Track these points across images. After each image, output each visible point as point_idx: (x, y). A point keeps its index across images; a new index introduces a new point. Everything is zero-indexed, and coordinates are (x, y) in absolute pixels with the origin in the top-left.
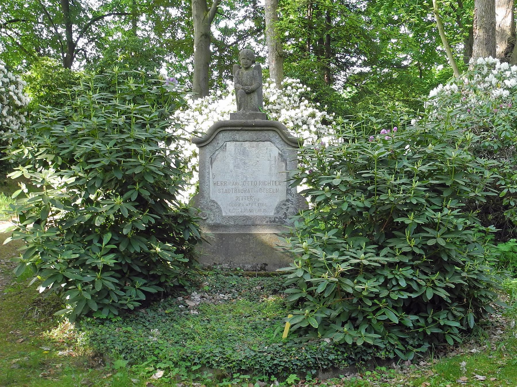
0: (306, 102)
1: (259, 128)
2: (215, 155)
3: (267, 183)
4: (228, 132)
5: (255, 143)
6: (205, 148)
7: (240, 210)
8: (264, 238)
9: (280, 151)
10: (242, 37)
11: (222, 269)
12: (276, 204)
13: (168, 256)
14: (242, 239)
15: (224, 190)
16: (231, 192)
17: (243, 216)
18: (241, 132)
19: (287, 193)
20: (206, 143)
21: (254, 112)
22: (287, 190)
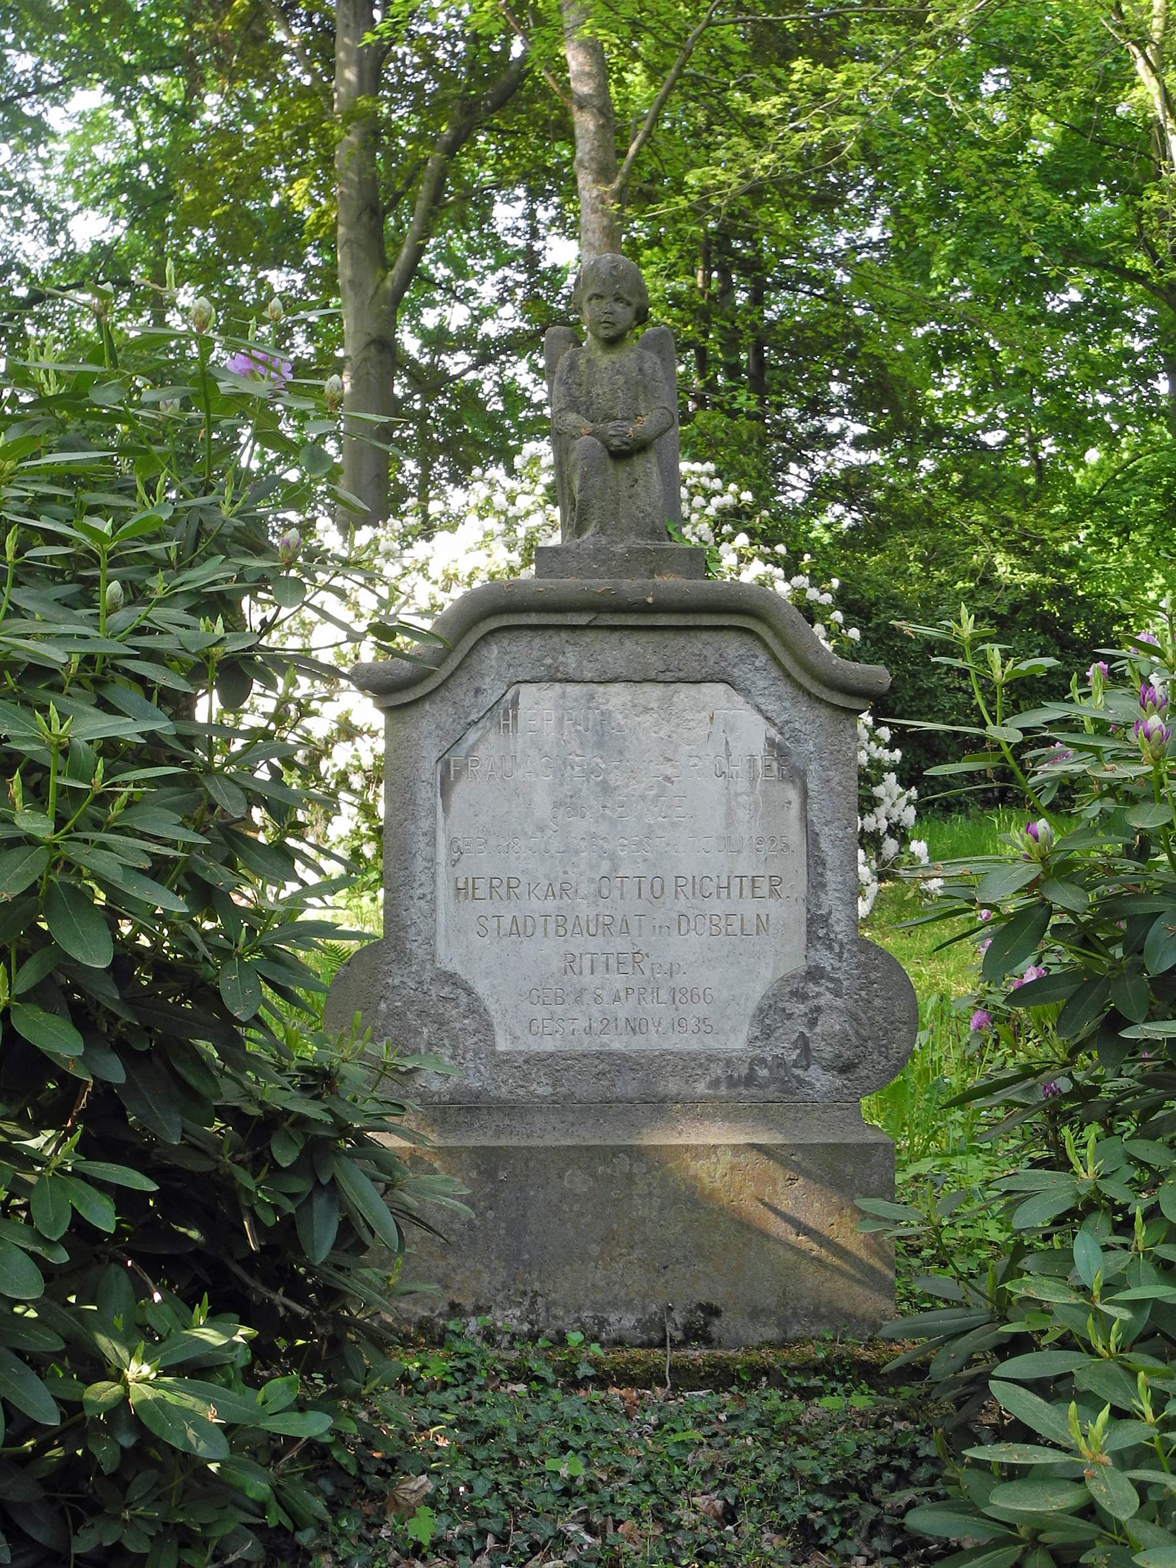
0: (742, 539)
1: (674, 620)
2: (465, 746)
3: (711, 887)
4: (527, 636)
5: (656, 691)
6: (414, 712)
7: (582, 1023)
8: (699, 1168)
9: (773, 732)
10: (487, 353)
11: (489, 1336)
12: (757, 991)
13: (199, 1423)
14: (593, 1175)
15: (506, 922)
16: (539, 932)
17: (599, 1055)
18: (589, 637)
19: (812, 938)
20: (419, 692)
21: (650, 544)
22: (811, 922)
